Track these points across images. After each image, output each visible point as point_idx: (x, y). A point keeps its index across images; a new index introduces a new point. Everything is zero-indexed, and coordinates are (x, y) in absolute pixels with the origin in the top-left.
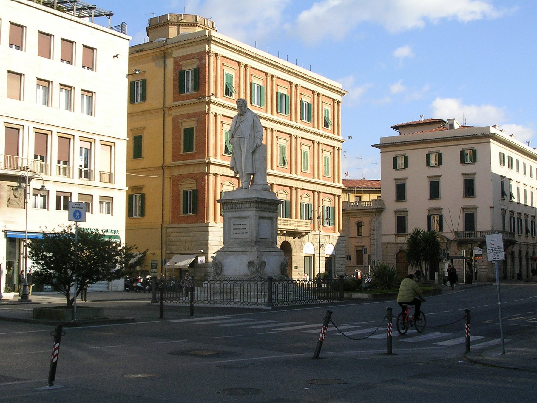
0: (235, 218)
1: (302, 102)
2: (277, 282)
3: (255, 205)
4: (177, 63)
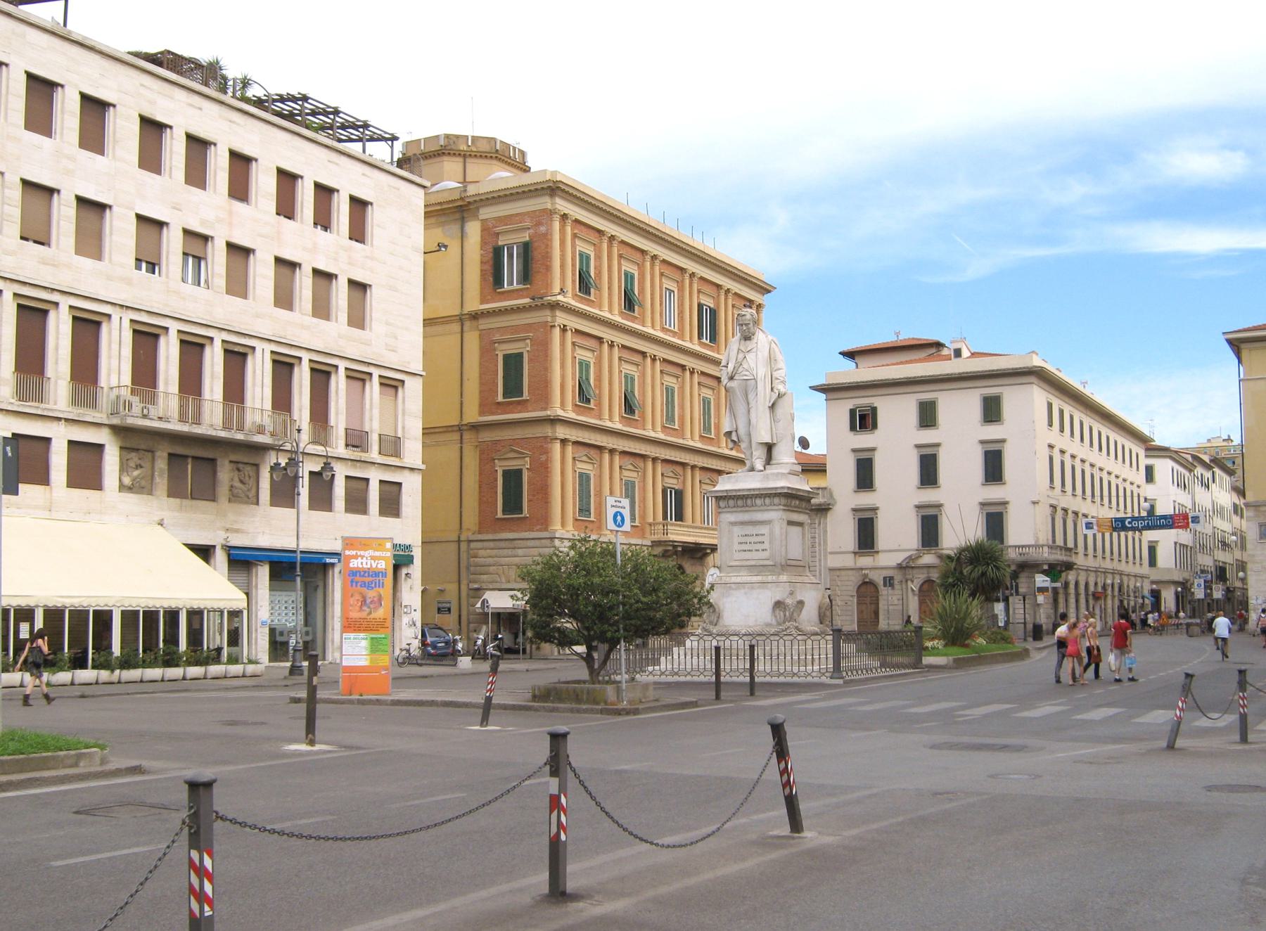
0: (743, 523)
1: (700, 306)
3: (783, 501)
4: (488, 232)
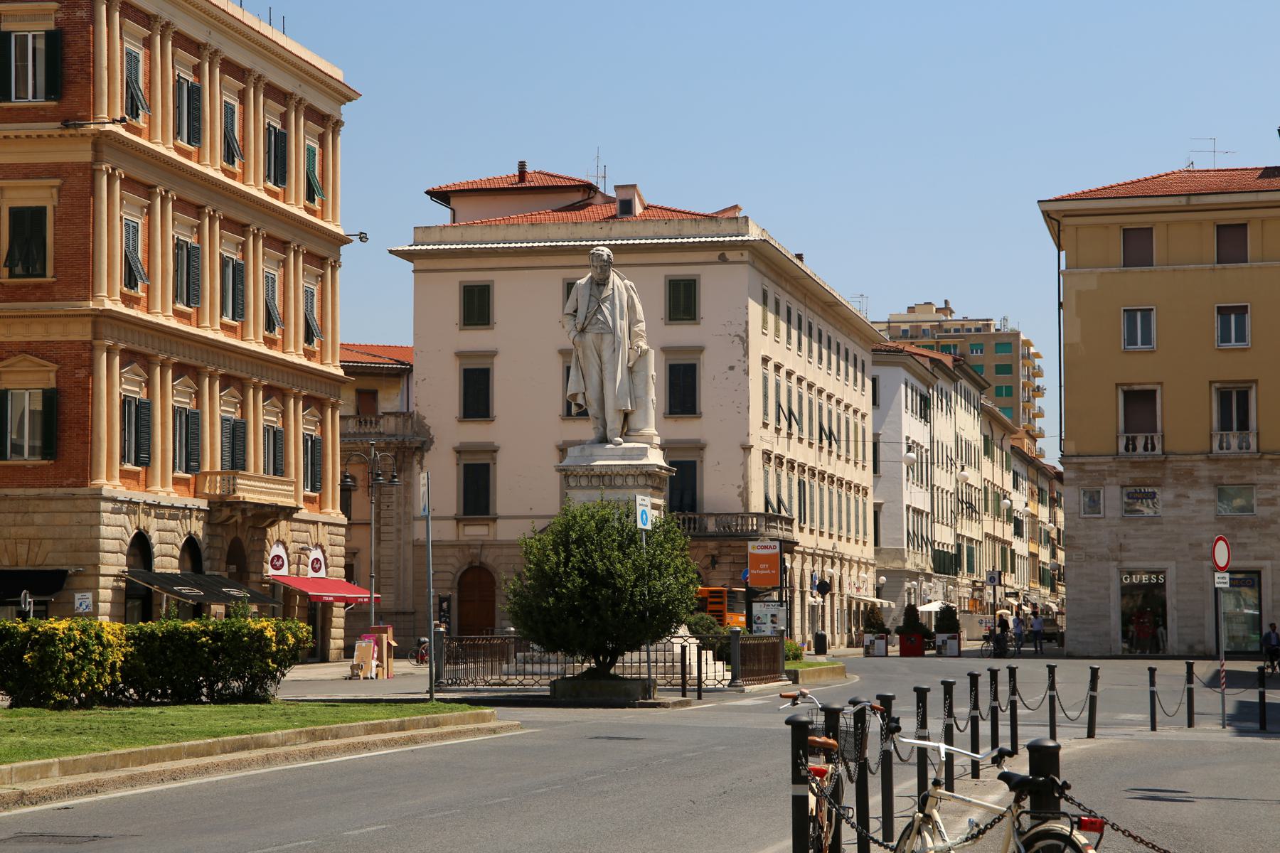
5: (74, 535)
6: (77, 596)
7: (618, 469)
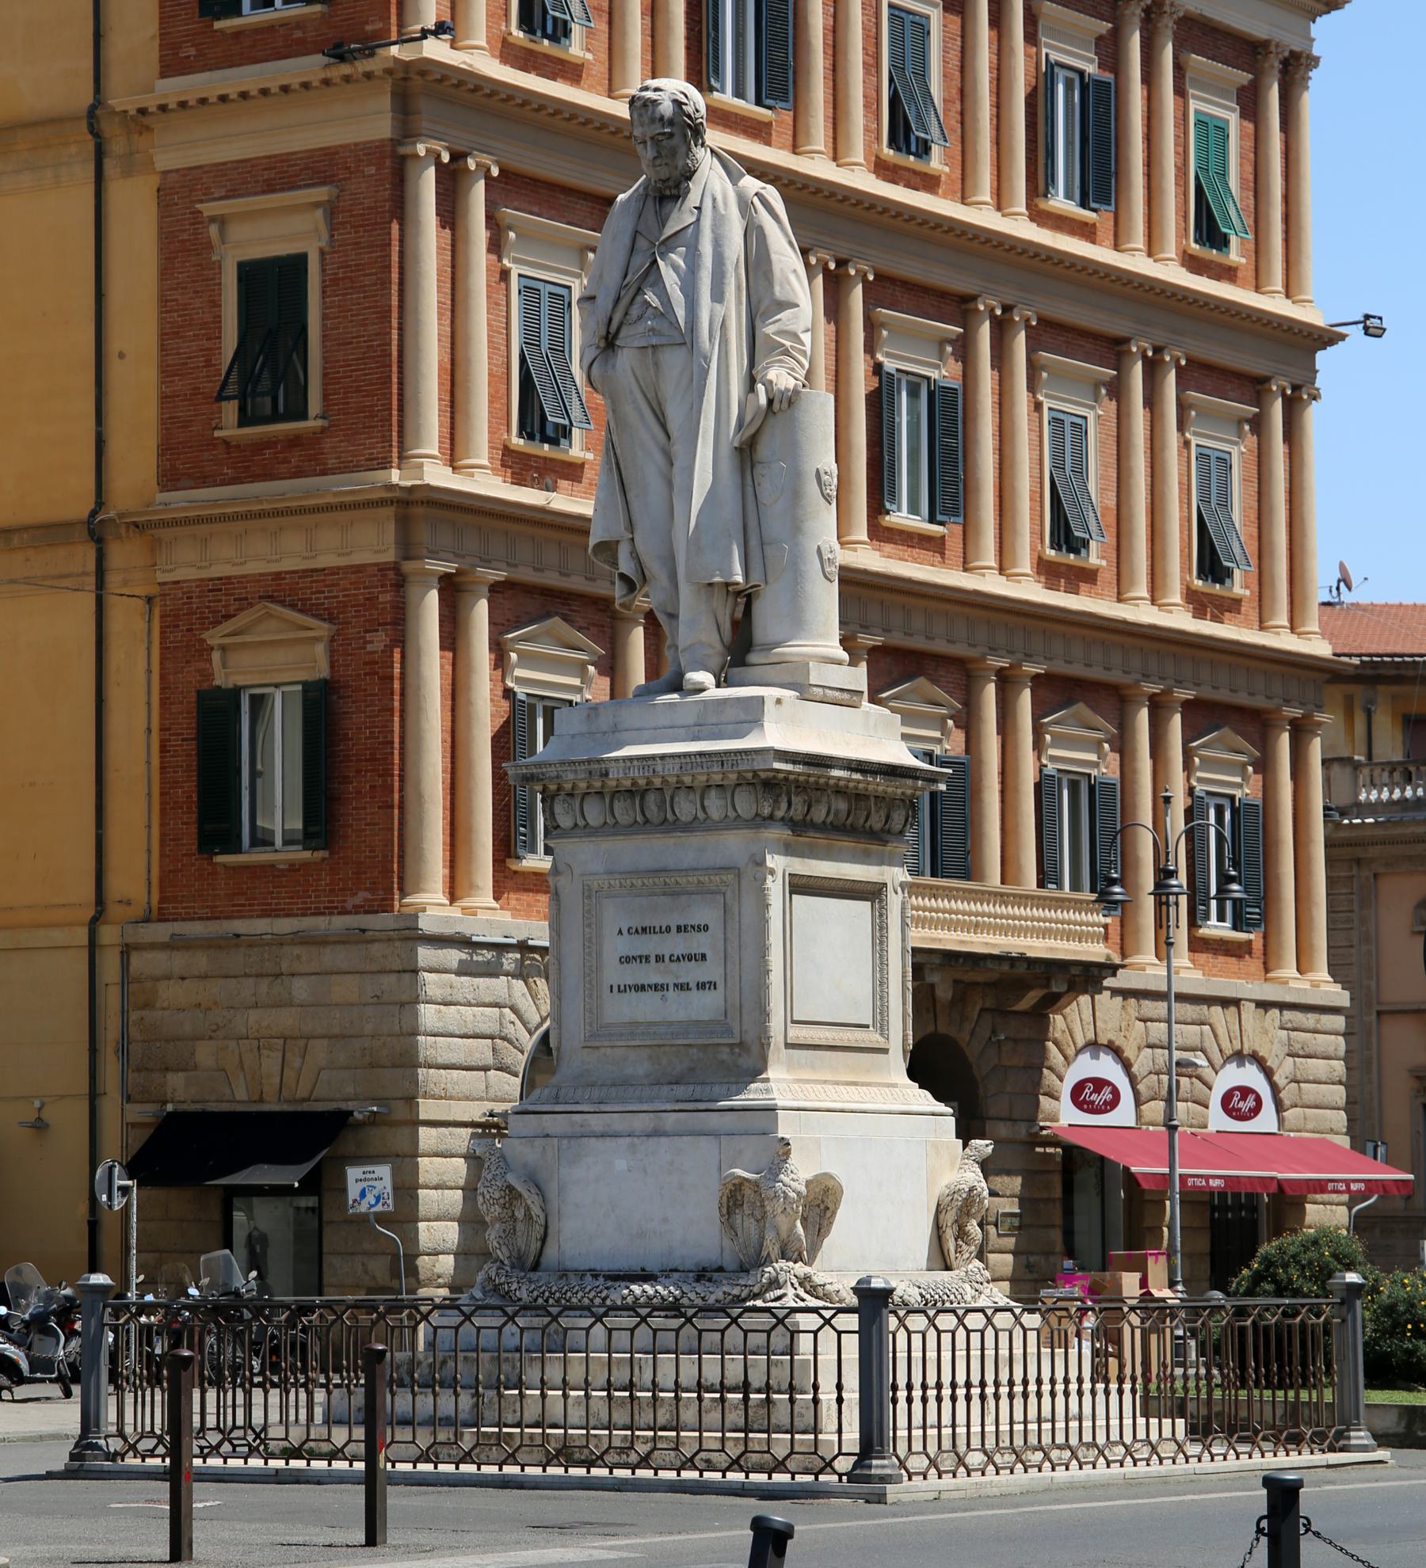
2: (917, 1322)
5: (369, 1028)
6: (353, 1173)
7: (671, 770)
